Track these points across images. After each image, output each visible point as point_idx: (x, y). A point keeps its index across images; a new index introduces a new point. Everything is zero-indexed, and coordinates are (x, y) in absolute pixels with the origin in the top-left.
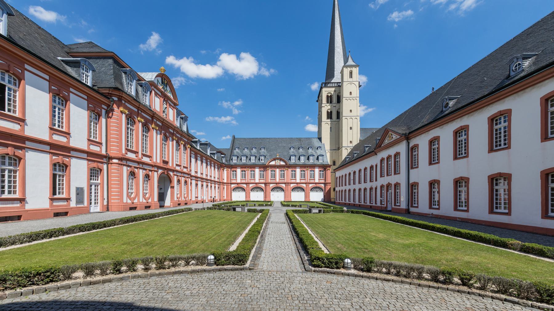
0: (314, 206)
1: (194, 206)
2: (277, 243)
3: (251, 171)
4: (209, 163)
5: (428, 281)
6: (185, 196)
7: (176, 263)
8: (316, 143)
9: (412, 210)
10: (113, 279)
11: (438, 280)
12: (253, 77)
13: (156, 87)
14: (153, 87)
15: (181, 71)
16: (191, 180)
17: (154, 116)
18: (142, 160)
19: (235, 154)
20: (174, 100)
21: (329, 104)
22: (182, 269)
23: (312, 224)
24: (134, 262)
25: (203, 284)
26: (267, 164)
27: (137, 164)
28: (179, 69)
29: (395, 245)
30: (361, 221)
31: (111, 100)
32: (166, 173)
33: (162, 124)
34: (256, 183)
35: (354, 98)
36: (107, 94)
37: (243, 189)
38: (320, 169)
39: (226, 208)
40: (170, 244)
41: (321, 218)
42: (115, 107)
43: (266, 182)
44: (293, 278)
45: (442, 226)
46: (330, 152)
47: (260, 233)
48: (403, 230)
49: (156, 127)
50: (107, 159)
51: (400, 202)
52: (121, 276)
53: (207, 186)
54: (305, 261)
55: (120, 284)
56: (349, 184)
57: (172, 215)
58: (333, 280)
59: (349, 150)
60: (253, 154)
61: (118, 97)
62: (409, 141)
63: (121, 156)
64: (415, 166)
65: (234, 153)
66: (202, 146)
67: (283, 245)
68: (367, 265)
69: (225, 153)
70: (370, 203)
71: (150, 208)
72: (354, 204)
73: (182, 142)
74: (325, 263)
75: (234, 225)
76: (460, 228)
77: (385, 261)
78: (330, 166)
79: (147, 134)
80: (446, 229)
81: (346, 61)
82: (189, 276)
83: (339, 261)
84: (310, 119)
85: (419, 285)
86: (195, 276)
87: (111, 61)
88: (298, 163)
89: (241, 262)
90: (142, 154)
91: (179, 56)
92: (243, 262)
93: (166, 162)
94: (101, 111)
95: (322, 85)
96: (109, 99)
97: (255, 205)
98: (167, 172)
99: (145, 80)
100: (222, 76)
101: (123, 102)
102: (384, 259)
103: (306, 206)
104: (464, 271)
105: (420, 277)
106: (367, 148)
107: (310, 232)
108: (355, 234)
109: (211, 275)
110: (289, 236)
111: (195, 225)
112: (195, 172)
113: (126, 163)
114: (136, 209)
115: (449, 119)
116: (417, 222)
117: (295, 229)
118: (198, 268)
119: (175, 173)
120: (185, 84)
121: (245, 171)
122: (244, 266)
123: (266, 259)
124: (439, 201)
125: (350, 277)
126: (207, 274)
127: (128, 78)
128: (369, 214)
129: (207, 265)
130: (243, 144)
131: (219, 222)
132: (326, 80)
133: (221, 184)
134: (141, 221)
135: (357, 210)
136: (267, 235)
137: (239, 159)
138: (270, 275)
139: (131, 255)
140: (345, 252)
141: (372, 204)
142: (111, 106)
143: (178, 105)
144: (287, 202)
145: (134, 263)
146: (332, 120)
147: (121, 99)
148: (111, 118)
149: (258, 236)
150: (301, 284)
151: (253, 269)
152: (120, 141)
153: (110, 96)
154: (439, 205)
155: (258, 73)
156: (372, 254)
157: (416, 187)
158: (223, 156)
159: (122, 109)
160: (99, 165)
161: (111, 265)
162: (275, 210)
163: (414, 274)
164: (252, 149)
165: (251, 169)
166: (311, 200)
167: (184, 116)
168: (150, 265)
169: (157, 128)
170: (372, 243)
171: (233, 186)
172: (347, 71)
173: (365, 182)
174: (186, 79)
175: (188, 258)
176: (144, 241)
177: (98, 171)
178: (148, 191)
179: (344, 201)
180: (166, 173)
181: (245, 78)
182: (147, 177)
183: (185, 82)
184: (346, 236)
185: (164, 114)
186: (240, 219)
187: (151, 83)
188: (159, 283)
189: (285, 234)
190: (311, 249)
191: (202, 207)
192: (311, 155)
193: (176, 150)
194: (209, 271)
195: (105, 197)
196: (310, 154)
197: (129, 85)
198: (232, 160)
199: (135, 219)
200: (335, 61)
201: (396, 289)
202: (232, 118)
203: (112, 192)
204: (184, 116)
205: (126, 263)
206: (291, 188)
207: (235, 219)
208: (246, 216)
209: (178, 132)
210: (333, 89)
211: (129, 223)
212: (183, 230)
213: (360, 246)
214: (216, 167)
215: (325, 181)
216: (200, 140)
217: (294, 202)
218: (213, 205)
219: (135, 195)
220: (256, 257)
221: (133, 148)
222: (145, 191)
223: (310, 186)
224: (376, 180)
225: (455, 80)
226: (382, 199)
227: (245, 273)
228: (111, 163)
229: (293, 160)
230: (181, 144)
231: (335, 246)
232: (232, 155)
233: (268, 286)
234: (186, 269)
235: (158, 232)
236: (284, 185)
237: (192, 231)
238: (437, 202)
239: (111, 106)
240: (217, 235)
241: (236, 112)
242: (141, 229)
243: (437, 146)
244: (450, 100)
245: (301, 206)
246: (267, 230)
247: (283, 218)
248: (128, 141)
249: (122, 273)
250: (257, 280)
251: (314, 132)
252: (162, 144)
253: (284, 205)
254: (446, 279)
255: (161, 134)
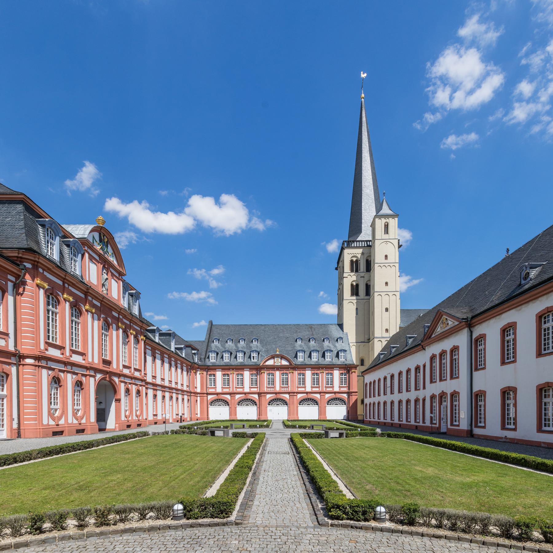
0: (332, 426)
1: (151, 429)
2: (277, 484)
3: (238, 375)
4: (173, 363)
5: (496, 537)
6: (138, 413)
7: (126, 517)
8: (335, 332)
9: (477, 431)
10: (31, 542)
11: (510, 536)
12: (239, 231)
13: (91, 247)
14: (86, 247)
15: (130, 222)
16: (147, 388)
17: (88, 292)
18: (71, 359)
19: (213, 349)
20: (118, 268)
21: (354, 274)
22: (135, 525)
23: (330, 454)
24: (62, 515)
25: (167, 547)
26: (261, 365)
27: (63, 365)
28: (125, 219)
29: (451, 485)
30: (401, 450)
31: (21, 267)
32: (108, 379)
33: (101, 303)
34: (245, 393)
35: (391, 265)
36: (16, 258)
37: (226, 403)
38: (341, 372)
39: (200, 431)
40: (116, 488)
41: (343, 445)
42: (28, 278)
43: (261, 392)
44: (300, 535)
45: (519, 455)
46: (356, 346)
47: (251, 469)
48: (462, 462)
49: (91, 309)
50: (17, 357)
51: (459, 420)
52: (43, 536)
53: (171, 398)
54: (318, 510)
55: (41, 549)
56: (385, 394)
57: (118, 443)
58: (359, 539)
59: (385, 343)
60: (240, 349)
61: (33, 262)
62: (472, 329)
63: (38, 353)
64: (481, 367)
65: (211, 347)
66: (162, 337)
67: (285, 486)
68: (408, 515)
69: (198, 347)
70: (415, 421)
71: (83, 432)
72: (392, 424)
73: (131, 331)
74: (348, 513)
75: (212, 457)
76: (545, 458)
77: (435, 509)
78: (355, 367)
79: (78, 319)
80: (524, 459)
81: (379, 207)
82: (145, 535)
83: (368, 510)
84: (325, 296)
85: (484, 543)
86: (155, 535)
87: (20, 207)
88: (308, 363)
89: (224, 514)
90: (71, 350)
91: (126, 199)
92: (226, 514)
93: (107, 363)
94: (7, 284)
95: (343, 244)
96: (18, 265)
97: (244, 426)
98: (110, 378)
99: (74, 237)
100: (194, 230)
101: (41, 270)
102: (434, 505)
103: (321, 428)
104: (548, 521)
105: (484, 532)
106: (411, 340)
107: (326, 467)
108: (393, 468)
109: (179, 533)
110: (295, 473)
111: (153, 458)
112: (153, 376)
113: (47, 364)
114: (62, 434)
115: (530, 297)
116: (483, 450)
117: (304, 463)
118: (159, 523)
119: (122, 379)
120: (136, 243)
121: (228, 375)
122: (228, 519)
123: (261, 509)
124: (515, 419)
125: (384, 533)
126: (172, 532)
127: (48, 234)
128: (413, 439)
129: (172, 519)
130: (224, 333)
131: (189, 453)
132: (349, 237)
133: (192, 394)
134: (70, 452)
135: (396, 433)
136: (262, 472)
137: (219, 356)
138: (266, 532)
139: (58, 505)
140: (377, 495)
141: (419, 422)
142: (22, 276)
143: (124, 275)
144: (292, 421)
145: (62, 517)
146: (358, 298)
147: (37, 266)
148: (22, 294)
149: (248, 474)
150: (313, 544)
151: (241, 524)
152: (37, 330)
153: (20, 261)
154: (515, 424)
155: (247, 226)
156: (417, 498)
157: (483, 398)
158: (195, 352)
159: (38, 281)
160: (4, 367)
161: (28, 522)
162: (275, 434)
163: (477, 527)
164: (239, 342)
165: (269, 372)
166: (328, 418)
167: (134, 291)
168: (87, 519)
169: (94, 311)
170: (417, 482)
171: (210, 397)
172: (380, 224)
173: (407, 391)
174: (137, 235)
175: (144, 509)
176: (76, 484)
177: (3, 377)
178: (80, 407)
179: (376, 420)
180: (108, 379)
181: (228, 233)
182: (78, 386)
183: (137, 239)
184: (380, 472)
185: (104, 289)
186: (222, 447)
187: (84, 242)
188: (101, 546)
189: (289, 471)
190: (327, 493)
191: (164, 431)
192: (327, 350)
193: (123, 343)
194: (176, 528)
195: (15, 415)
196: (326, 348)
197: (49, 244)
198: (208, 358)
199: (61, 449)
200: (363, 209)
201: (451, 549)
202: (209, 293)
203: (24, 408)
204: (134, 291)
205: (50, 517)
206: (297, 400)
207: (214, 448)
208: (231, 443)
209: (125, 317)
210: (360, 251)
211: (52, 456)
212: (135, 466)
213: (399, 487)
214: (185, 368)
215: (349, 389)
216: (160, 328)
217: (302, 421)
218: (181, 427)
219: (60, 413)
220: (245, 506)
221: (56, 341)
222: (76, 407)
223: (326, 397)
224: (424, 388)
225: (539, 238)
226: (433, 415)
227: (229, 530)
228: (23, 365)
229: (301, 359)
230: (131, 334)
231: (363, 486)
232: (208, 350)
233: (263, 548)
234: (141, 525)
235: (97, 469)
236: (287, 396)
237: (150, 467)
238: (512, 419)
239: (22, 276)
240: (187, 473)
241: (214, 285)
242: (71, 465)
243: (512, 337)
244: (531, 268)
245: (313, 426)
246: (262, 464)
247: (286, 446)
248: (49, 330)
249: (44, 532)
250: (247, 539)
251: (331, 316)
252: (101, 334)
253: (287, 426)
254: (522, 533)
255: (99, 320)
